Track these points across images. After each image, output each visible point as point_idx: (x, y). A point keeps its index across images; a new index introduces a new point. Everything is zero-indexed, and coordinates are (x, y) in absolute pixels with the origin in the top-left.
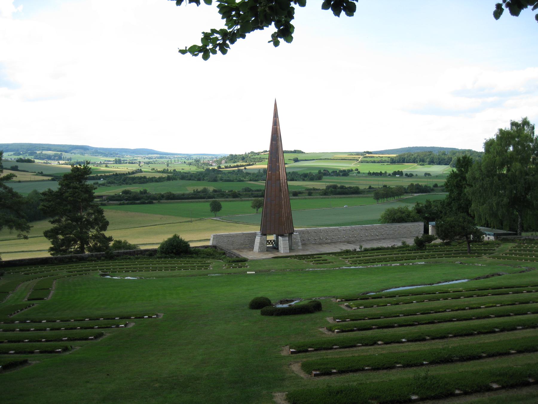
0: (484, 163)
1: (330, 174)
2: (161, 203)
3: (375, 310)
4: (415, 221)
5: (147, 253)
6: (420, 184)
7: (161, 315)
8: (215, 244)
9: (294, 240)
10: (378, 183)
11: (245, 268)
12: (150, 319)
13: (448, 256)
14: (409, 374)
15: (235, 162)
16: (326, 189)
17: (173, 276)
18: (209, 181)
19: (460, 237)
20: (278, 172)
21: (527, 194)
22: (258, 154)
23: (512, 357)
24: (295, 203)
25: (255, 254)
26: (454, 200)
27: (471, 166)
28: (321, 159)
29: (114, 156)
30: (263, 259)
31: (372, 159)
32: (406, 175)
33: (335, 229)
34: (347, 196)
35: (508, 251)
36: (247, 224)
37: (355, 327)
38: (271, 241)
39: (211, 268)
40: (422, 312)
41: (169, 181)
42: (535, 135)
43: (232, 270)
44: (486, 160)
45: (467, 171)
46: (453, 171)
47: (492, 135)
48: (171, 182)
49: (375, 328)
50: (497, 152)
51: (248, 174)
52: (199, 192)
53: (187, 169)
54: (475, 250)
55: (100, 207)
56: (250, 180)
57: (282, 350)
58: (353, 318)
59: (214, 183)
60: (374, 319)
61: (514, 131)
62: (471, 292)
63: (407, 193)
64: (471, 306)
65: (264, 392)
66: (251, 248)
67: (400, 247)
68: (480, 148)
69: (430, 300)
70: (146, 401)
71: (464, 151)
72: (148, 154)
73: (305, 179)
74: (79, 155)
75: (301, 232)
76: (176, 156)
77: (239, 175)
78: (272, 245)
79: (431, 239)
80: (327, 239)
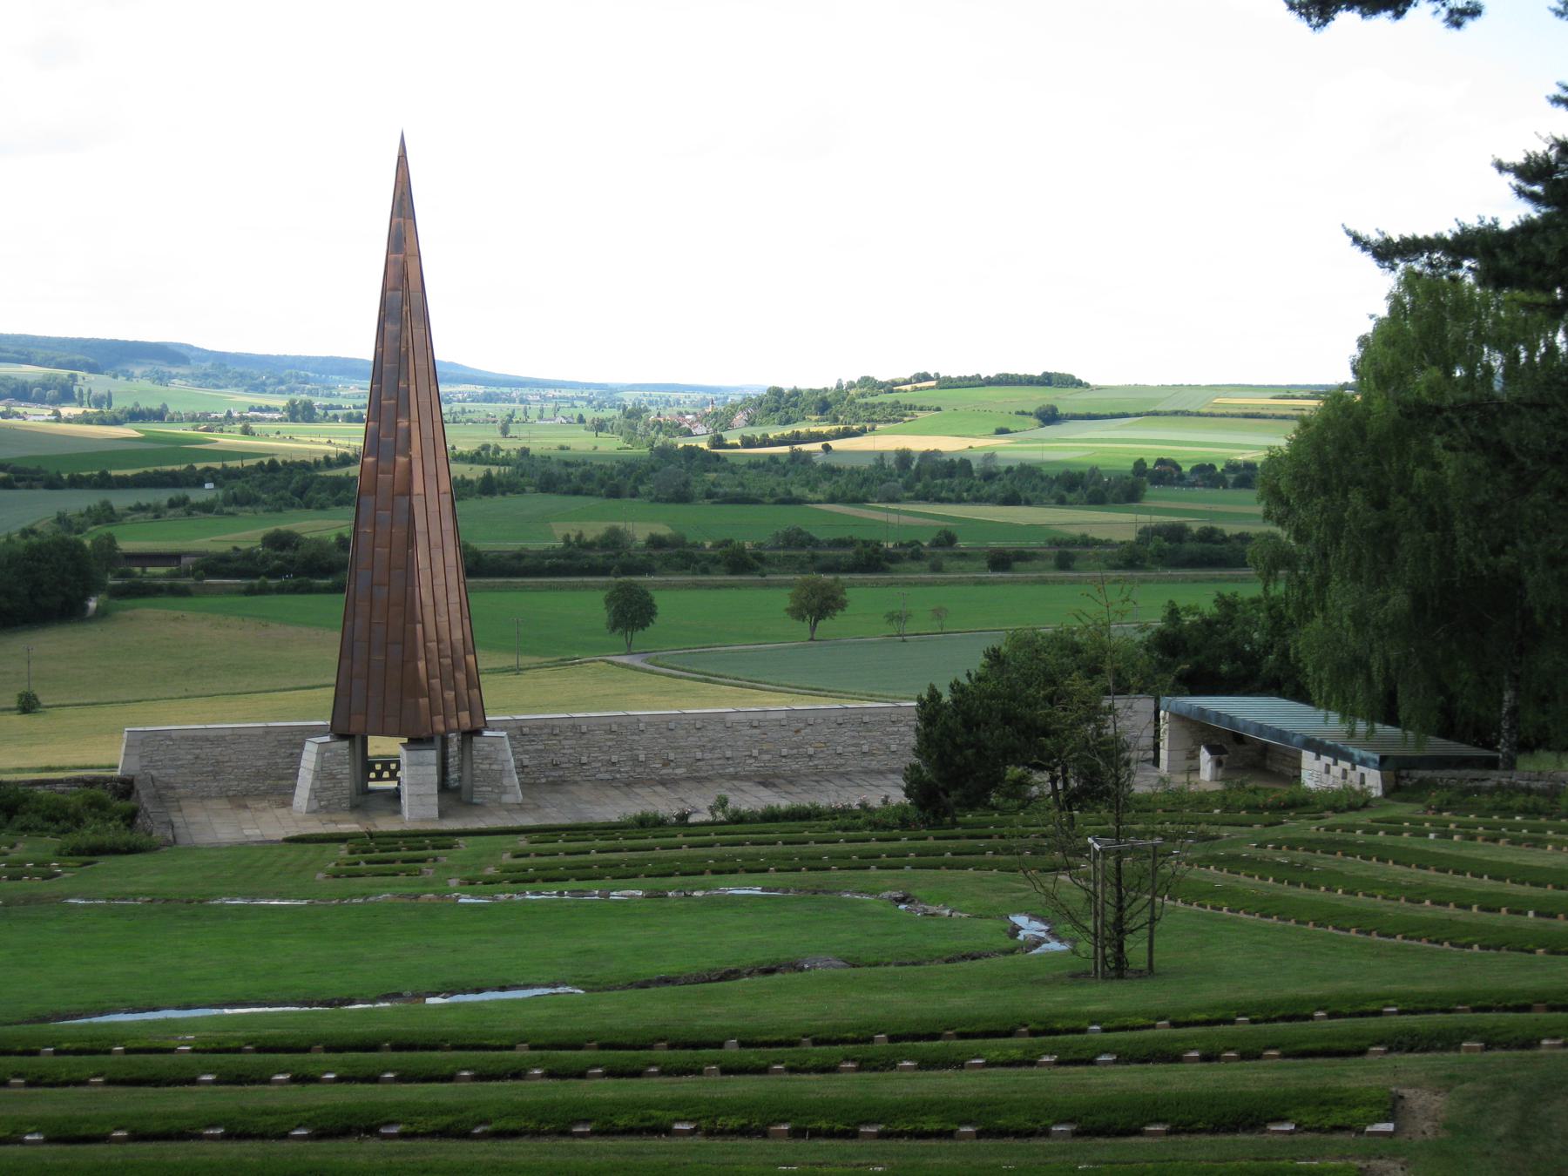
1: (1182, 477)
15: (788, 422)
16: (1138, 542)
18: (657, 500)
22: (889, 387)
28: (1156, 414)
34: (1215, 573)
48: (497, 503)
51: (831, 471)
52: (590, 546)
53: (582, 442)
66: (282, 794)
73: (1070, 497)
74: (145, 384)
75: (520, 734)
76: (551, 393)
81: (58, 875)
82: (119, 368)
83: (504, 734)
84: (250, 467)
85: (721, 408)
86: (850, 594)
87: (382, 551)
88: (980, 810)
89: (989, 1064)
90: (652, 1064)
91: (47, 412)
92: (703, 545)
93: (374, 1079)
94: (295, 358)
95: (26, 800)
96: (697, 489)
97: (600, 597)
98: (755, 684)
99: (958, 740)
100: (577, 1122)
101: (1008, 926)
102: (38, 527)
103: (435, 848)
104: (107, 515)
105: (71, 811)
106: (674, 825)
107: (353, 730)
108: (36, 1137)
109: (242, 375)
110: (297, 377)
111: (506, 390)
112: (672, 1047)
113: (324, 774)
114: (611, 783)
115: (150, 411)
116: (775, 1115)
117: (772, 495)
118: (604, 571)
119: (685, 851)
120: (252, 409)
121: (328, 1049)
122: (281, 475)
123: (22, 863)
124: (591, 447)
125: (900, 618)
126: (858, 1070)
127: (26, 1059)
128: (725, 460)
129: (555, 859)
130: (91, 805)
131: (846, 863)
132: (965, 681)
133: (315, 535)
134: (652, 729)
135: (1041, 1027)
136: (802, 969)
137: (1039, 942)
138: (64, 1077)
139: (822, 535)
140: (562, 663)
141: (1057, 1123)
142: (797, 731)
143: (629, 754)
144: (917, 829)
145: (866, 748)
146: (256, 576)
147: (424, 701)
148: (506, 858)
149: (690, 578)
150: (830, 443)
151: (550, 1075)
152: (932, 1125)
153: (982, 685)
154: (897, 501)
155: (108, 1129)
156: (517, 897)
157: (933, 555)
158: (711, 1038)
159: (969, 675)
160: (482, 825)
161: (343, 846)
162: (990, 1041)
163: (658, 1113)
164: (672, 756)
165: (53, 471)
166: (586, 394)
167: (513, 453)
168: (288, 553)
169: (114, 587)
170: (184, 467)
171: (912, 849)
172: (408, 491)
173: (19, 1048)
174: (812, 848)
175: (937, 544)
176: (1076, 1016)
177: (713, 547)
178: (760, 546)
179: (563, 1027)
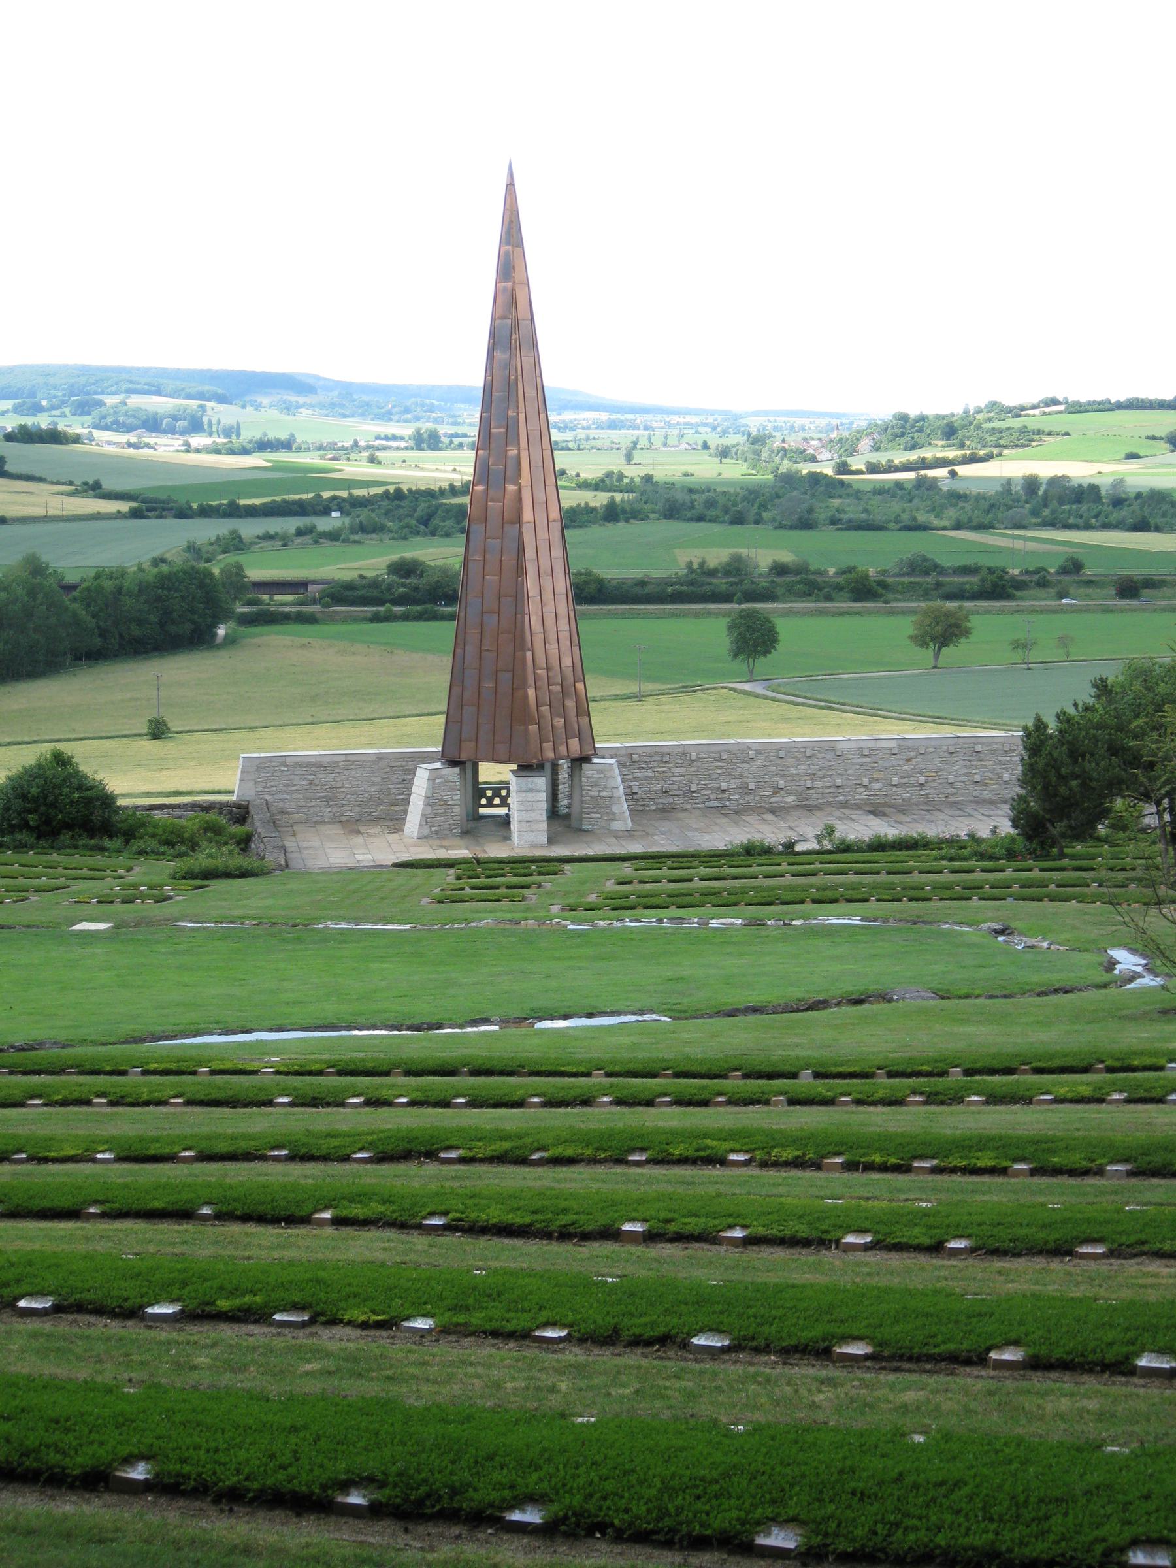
15: (914, 447)
18: (781, 526)
22: (1018, 412)
34: (712, 606)
41: (609, 525)
48: (621, 529)
51: (957, 497)
52: (712, 573)
53: (707, 469)
56: (958, 526)
66: (394, 819)
74: (274, 414)
75: (630, 761)
76: (675, 419)
80: (776, 791)
81: (170, 898)
82: (247, 398)
83: (613, 761)
84: (375, 495)
85: (846, 434)
86: (975, 622)
87: (491, 579)
88: (1091, 843)
89: (1058, 1101)
90: (720, 1094)
91: (177, 442)
92: (826, 572)
93: (445, 1104)
94: (420, 387)
95: (143, 825)
96: (821, 515)
97: (723, 622)
98: (876, 711)
99: (1063, 771)
100: (633, 1150)
101: (1105, 960)
102: (168, 556)
103: (540, 874)
104: (236, 544)
105: (186, 835)
106: (780, 853)
107: (464, 756)
108: (107, 1156)
109: (368, 404)
110: (423, 405)
111: (630, 416)
112: (746, 1076)
113: (434, 800)
114: (721, 810)
115: (278, 440)
116: (830, 1148)
118: (726, 598)
119: (788, 880)
120: (378, 438)
121: (408, 1073)
122: (405, 503)
123: (135, 887)
124: (715, 474)
125: (1024, 646)
126: (925, 1103)
127: (114, 1078)
128: (850, 486)
129: (690, 885)
130: (206, 830)
131: (948, 894)
132: (1072, 711)
133: (439, 563)
134: (762, 757)
135: (1117, 1064)
136: (890, 1000)
137: (1133, 977)
138: (145, 1097)
139: (947, 562)
140: (685, 690)
141: (1111, 1162)
142: (908, 760)
143: (735, 781)
144: (1024, 859)
145: (977, 777)
146: (381, 603)
147: (533, 728)
148: (610, 886)
149: (813, 605)
150: (957, 468)
151: (619, 1102)
152: (986, 1162)
153: (1089, 715)
154: (1024, 527)
155: (176, 1149)
156: (616, 924)
157: (1060, 582)
158: (787, 1068)
159: (1076, 705)
160: (590, 852)
161: (451, 871)
162: (1065, 1077)
163: (715, 1143)
164: (782, 784)
165: (182, 501)
166: (710, 420)
167: (637, 480)
168: (413, 581)
169: (243, 614)
170: (311, 495)
171: (1016, 881)
172: (519, 520)
173: (108, 1068)
174: (916, 878)
175: (1064, 571)
176: (1151, 1054)
177: (837, 573)
178: (884, 572)
179: (641, 1055)
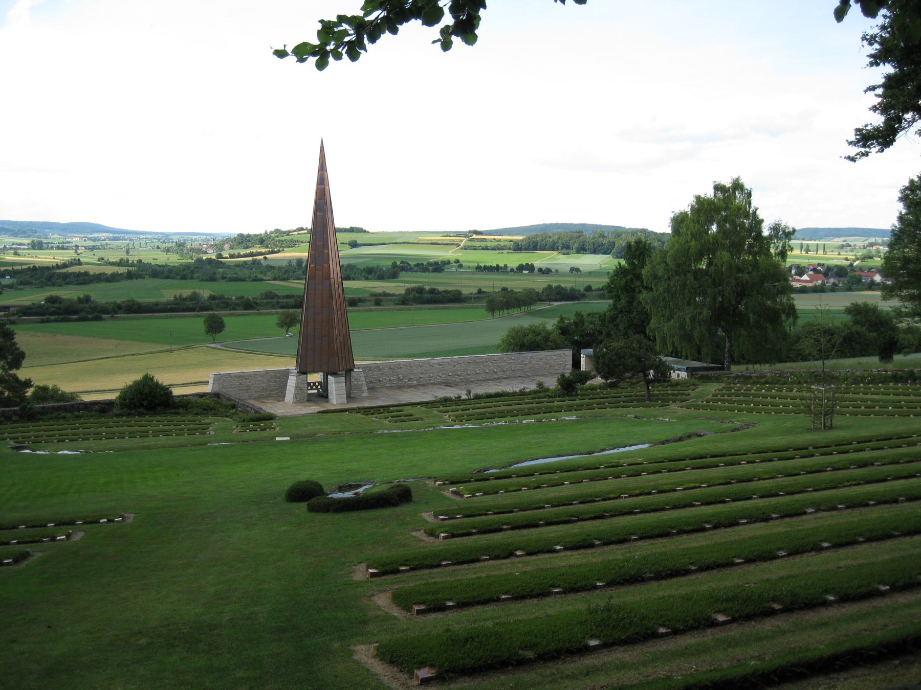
0: (671, 252)
1: (411, 268)
2: (117, 318)
3: (503, 499)
4: (557, 347)
5: (97, 407)
6: (563, 285)
7: (131, 517)
8: (217, 390)
9: (354, 382)
10: (492, 284)
11: (272, 432)
12: (111, 524)
13: (615, 405)
14: (576, 604)
15: (247, 247)
16: (406, 294)
17: (144, 448)
18: (202, 280)
19: (633, 375)
20: (326, 265)
21: (739, 303)
22: (288, 233)
23: (738, 570)
24: (355, 318)
25: (287, 406)
26: (621, 312)
27: (650, 256)
28: (396, 243)
29: (29, 236)
30: (303, 415)
31: (483, 244)
32: (540, 270)
33: (424, 362)
34: (437, 306)
35: (710, 397)
36: (270, 354)
37: (474, 528)
38: (314, 383)
39: (213, 433)
40: (581, 500)
41: (129, 281)
42: (752, 206)
43: (248, 435)
44: (674, 246)
45: (643, 265)
46: (620, 264)
47: (684, 205)
48: (134, 282)
49: (506, 530)
50: (692, 234)
51: (270, 268)
52: (185, 300)
53: (162, 259)
54: (658, 395)
55: (7, 326)
56: (275, 279)
57: (354, 572)
58: (468, 513)
59: (209, 283)
60: (503, 513)
61: (719, 199)
62: (658, 465)
63: (541, 300)
64: (660, 488)
65: (336, 645)
66: (281, 396)
67: (535, 392)
68: (663, 227)
69: (592, 480)
70: (128, 671)
71: (634, 232)
72: (92, 232)
73: (370, 276)
75: (366, 368)
76: (142, 236)
77: (255, 271)
78: (316, 391)
79: (585, 377)
97: (201, 320)
117: (249, 277)
139: (280, 294)
140: (187, 348)
178: (255, 298)
